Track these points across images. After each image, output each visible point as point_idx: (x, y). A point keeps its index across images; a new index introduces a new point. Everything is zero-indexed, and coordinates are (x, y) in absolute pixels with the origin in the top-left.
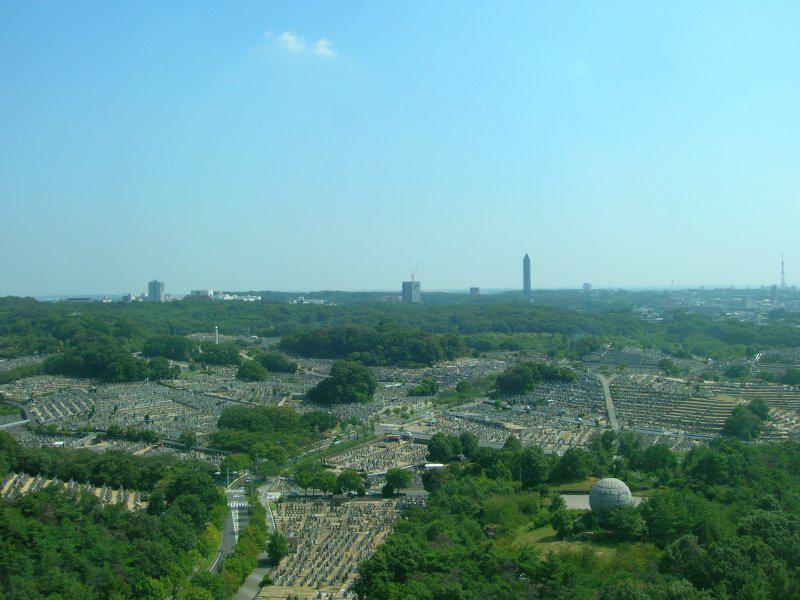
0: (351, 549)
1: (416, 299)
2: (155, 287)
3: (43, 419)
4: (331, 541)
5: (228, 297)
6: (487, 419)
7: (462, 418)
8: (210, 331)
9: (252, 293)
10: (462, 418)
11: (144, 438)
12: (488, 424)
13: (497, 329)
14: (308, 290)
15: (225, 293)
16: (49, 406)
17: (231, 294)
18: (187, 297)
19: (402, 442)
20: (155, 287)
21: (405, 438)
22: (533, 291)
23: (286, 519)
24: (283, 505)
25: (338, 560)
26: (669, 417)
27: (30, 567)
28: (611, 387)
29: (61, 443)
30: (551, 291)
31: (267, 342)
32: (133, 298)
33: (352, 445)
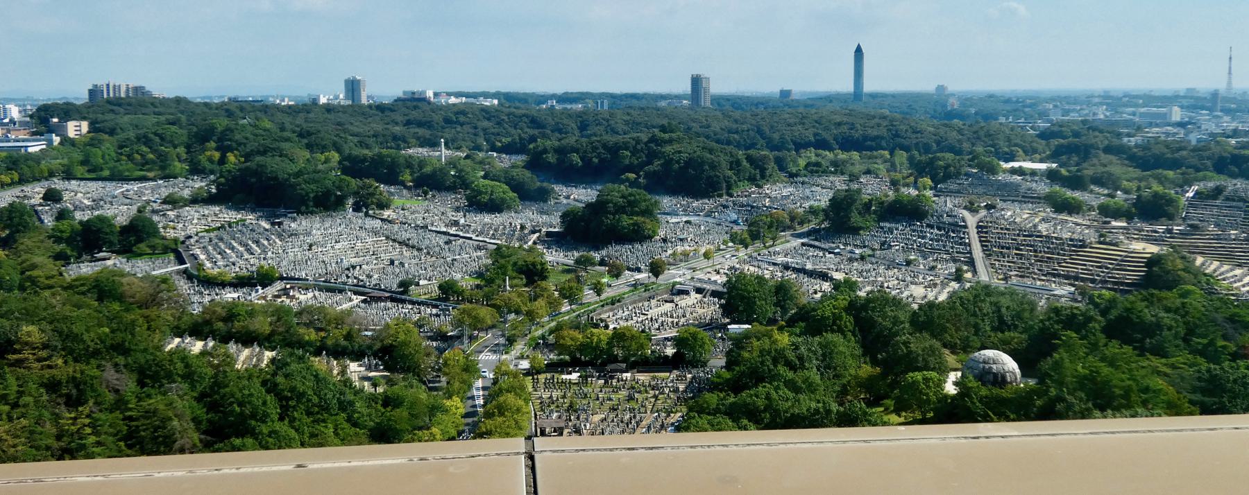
1: (706, 102)
2: (353, 87)
3: (208, 265)
5: (453, 100)
6: (809, 266)
7: (774, 264)
8: (434, 144)
9: (486, 95)
10: (774, 264)
11: (119, 401)
15: (449, 94)
16: (216, 247)
17: (458, 95)
18: (398, 100)
20: (353, 87)
24: (542, 377)
26: (1062, 271)
28: (978, 227)
29: (235, 295)
30: (893, 96)
32: (323, 100)
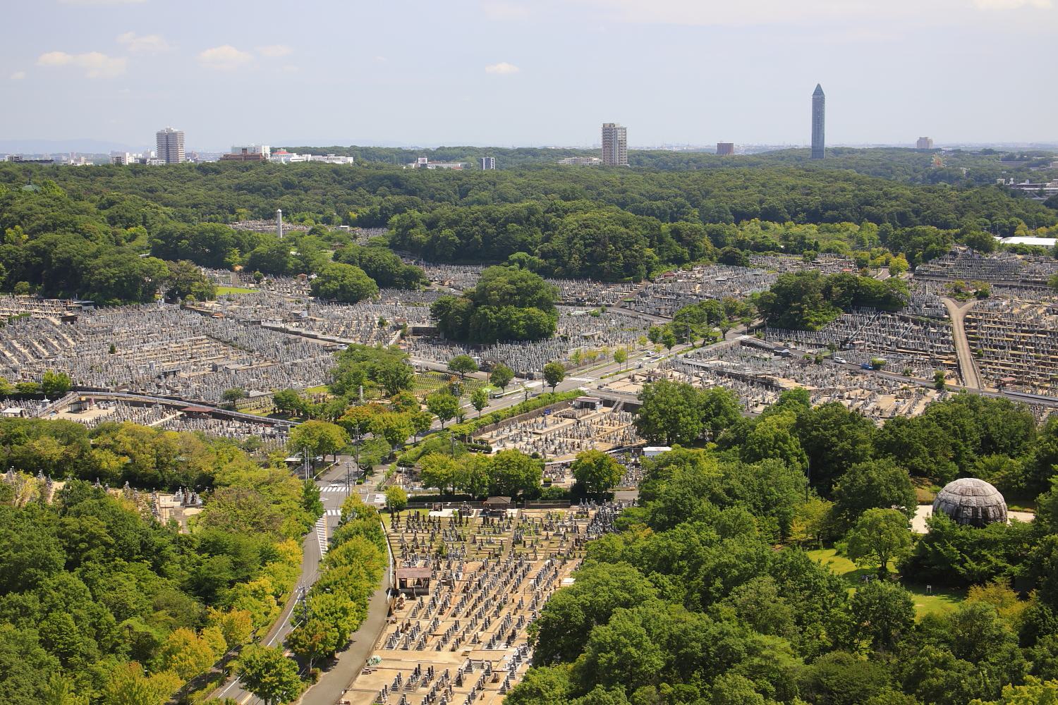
0: (521, 590)
2: (168, 142)
4: (487, 576)
5: (295, 158)
6: (749, 371)
7: (705, 369)
9: (338, 151)
12: (752, 381)
13: (770, 215)
14: (433, 143)
15: (290, 150)
17: (301, 151)
19: (601, 409)
20: (168, 142)
21: (607, 403)
22: (827, 150)
23: (408, 538)
25: (500, 608)
27: (840, 653)
28: (966, 320)
29: (18, 410)
30: (863, 151)
31: (365, 236)
33: (529, 411)
